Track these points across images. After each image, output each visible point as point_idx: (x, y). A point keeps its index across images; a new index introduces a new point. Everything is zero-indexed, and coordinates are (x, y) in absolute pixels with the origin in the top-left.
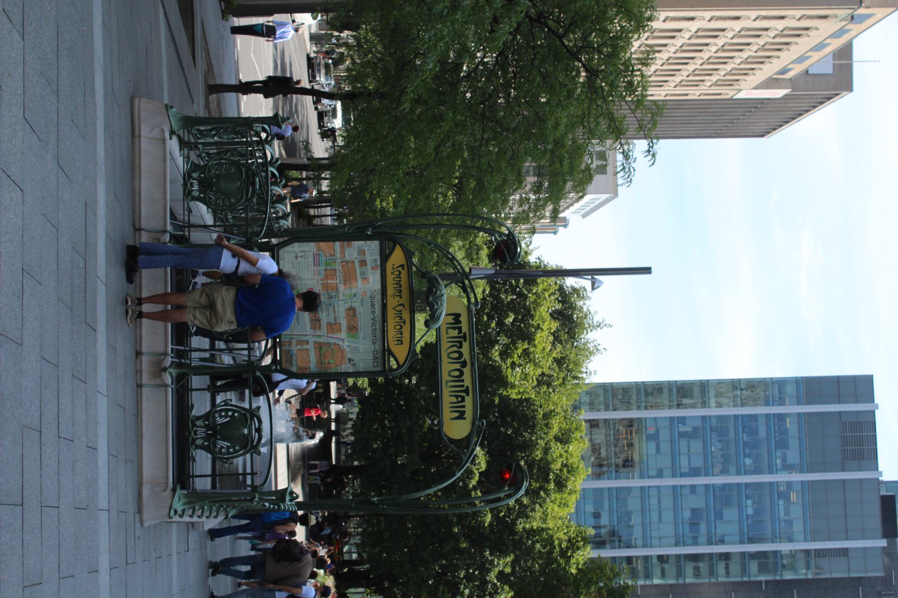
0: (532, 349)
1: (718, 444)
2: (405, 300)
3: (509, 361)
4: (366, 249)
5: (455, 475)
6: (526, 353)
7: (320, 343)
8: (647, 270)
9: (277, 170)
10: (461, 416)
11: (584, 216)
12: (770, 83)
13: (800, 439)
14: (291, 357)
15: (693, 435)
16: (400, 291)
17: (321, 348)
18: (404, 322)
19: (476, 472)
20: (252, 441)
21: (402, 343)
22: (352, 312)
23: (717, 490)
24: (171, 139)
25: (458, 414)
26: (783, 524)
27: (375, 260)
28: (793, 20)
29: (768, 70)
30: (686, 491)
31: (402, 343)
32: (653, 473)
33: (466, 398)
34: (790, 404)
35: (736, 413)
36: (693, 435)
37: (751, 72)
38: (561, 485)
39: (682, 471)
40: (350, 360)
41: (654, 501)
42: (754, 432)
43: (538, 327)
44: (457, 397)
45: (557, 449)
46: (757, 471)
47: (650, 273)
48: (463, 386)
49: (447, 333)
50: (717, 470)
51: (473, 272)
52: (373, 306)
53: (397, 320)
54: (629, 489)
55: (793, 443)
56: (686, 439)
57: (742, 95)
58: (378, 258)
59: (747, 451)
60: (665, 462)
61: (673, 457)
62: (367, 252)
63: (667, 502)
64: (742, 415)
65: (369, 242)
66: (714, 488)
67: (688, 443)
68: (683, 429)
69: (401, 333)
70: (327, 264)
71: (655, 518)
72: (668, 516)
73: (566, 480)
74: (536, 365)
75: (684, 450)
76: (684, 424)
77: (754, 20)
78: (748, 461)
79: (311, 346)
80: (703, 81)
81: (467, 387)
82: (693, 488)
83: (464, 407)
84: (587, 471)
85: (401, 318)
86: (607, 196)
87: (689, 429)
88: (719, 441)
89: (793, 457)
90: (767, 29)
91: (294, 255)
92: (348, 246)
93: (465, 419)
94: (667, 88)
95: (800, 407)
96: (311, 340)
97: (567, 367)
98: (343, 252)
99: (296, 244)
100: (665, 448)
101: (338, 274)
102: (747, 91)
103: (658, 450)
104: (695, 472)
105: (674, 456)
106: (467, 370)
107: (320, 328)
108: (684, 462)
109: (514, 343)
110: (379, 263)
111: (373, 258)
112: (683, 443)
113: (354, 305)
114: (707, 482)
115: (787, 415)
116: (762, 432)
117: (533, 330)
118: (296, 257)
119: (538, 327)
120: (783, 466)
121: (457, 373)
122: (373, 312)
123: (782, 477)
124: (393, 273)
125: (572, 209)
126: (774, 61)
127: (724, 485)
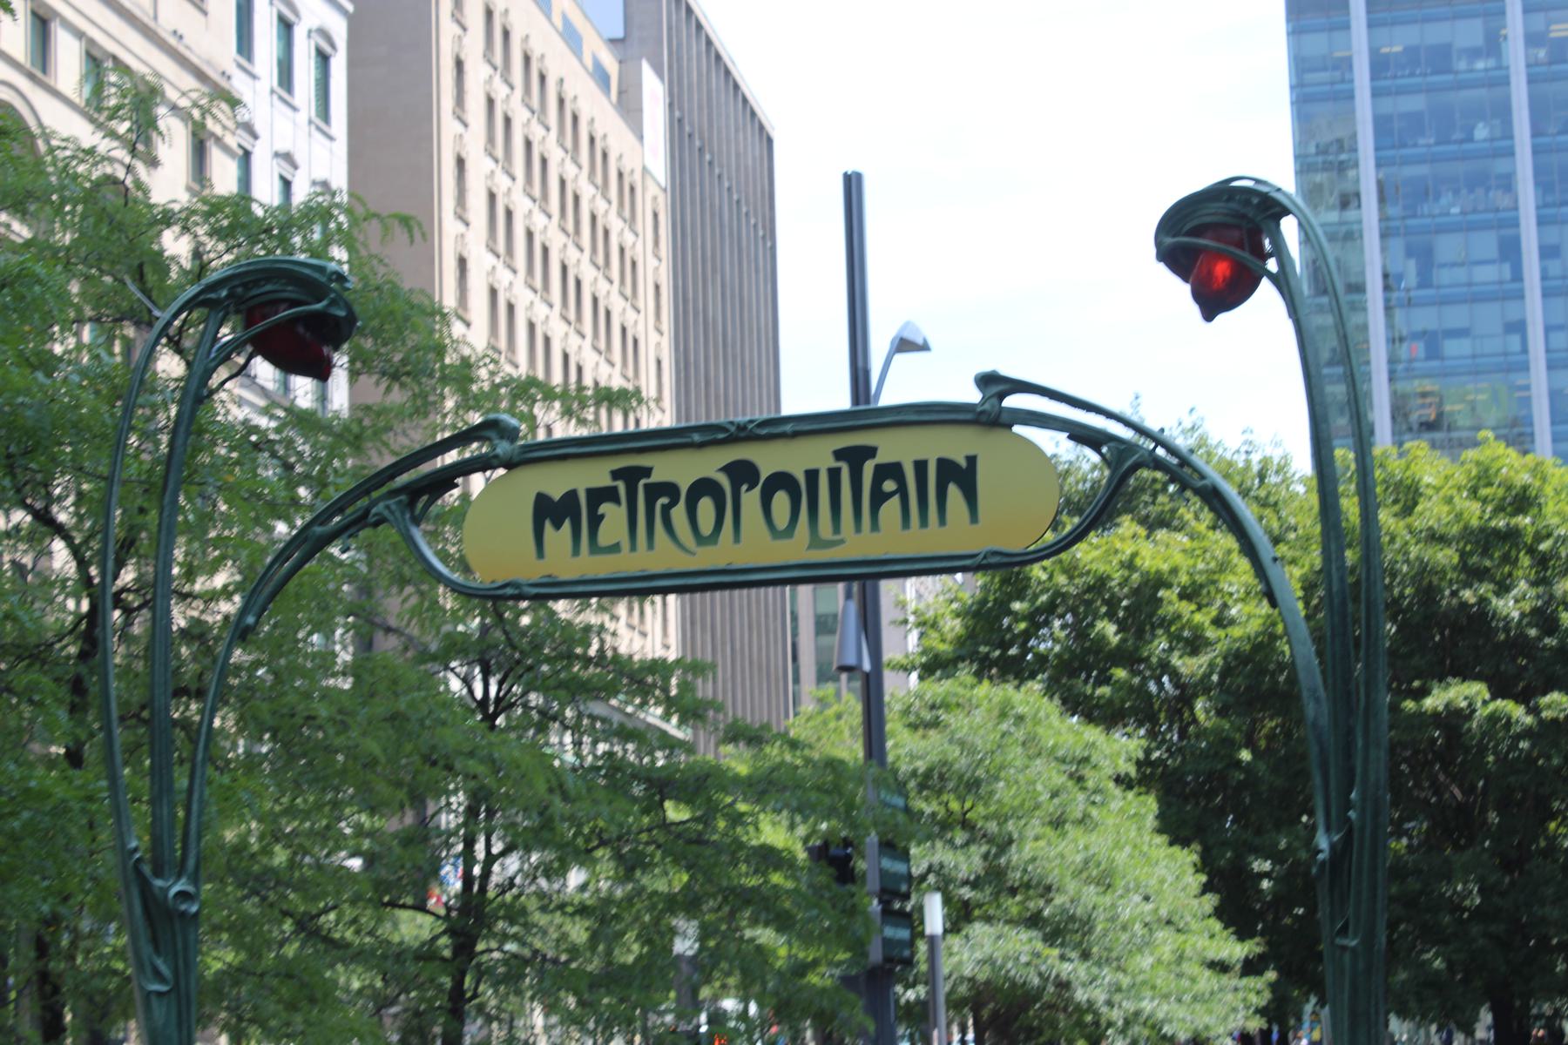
0: (1184, 579)
1: (1444, 201)
3: (1211, 633)
6: (1190, 594)
8: (852, 186)
12: (629, 106)
13: (1427, 20)
15: (1425, 258)
19: (1491, 707)
23: (1549, 199)
25: (953, 491)
28: (466, 40)
29: (596, 109)
30: (1555, 267)
32: (1514, 342)
33: (881, 458)
34: (1349, 47)
35: (1371, 163)
36: (1425, 258)
37: (599, 145)
38: (1522, 501)
39: (1507, 274)
42: (1415, 122)
43: (1130, 565)
44: (879, 498)
45: (1431, 512)
46: (1503, 112)
47: (859, 176)
48: (834, 474)
49: (615, 548)
50: (1504, 201)
51: (851, 660)
55: (1436, 34)
56: (1435, 271)
57: (658, 164)
59: (1457, 135)
60: (1489, 317)
64: (1377, 149)
66: (1546, 206)
67: (1444, 265)
68: (1411, 279)
73: (1509, 488)
74: (1224, 567)
75: (1460, 274)
76: (1400, 277)
77: (466, 125)
78: (1481, 132)
80: (622, 250)
81: (839, 454)
83: (921, 466)
84: (1486, 440)
87: (1411, 268)
88: (1437, 198)
89: (1469, 33)
90: (491, 102)
93: (972, 460)
94: (641, 327)
95: (1354, 24)
100: (1456, 317)
102: (648, 154)
104: (1510, 250)
105: (1476, 297)
108: (1487, 274)
109: (1165, 623)
112: (1444, 276)
114: (1533, 221)
115: (1374, 53)
116: (1415, 103)
117: (1135, 576)
119: (1130, 565)
120: (1488, 55)
121: (781, 500)
123: (1516, 55)
127: (1537, 184)
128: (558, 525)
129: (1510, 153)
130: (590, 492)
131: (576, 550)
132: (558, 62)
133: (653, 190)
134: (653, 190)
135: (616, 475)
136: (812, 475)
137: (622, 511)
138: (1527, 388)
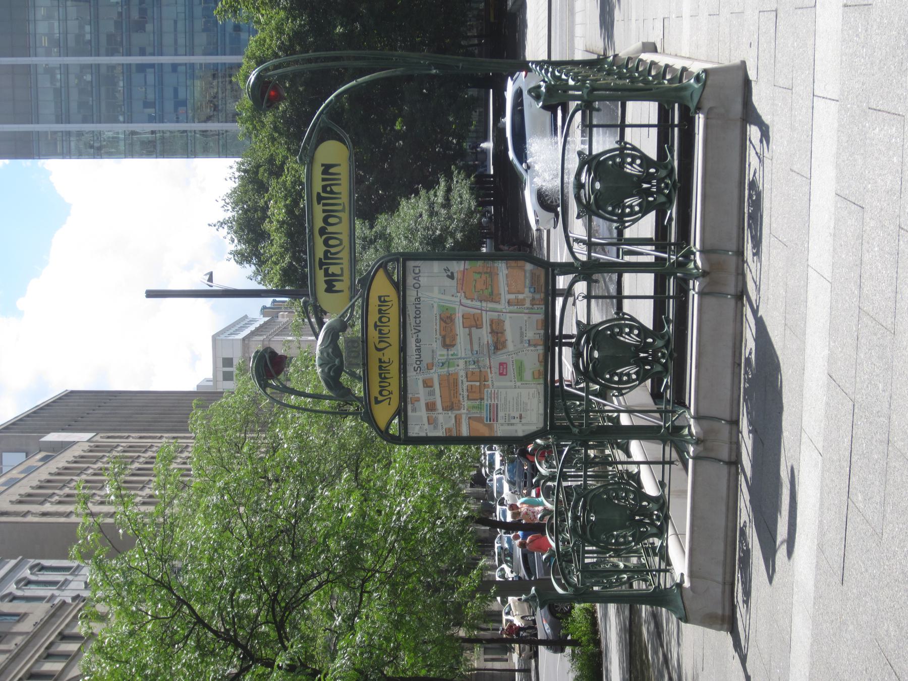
2: (374, 356)
4: (426, 426)
5: (336, 96)
7: (492, 301)
8: (151, 294)
9: (538, 470)
10: (327, 168)
11: (246, 317)
14: (532, 284)
16: (380, 368)
17: (492, 294)
18: (376, 326)
20: (589, 171)
21: (380, 297)
22: (448, 342)
24: (682, 575)
25: (331, 171)
26: (56, 14)
27: (414, 410)
29: (61, 461)
30: (149, 49)
31: (380, 297)
32: (180, 69)
33: (320, 191)
37: (78, 459)
39: (152, 70)
40: (451, 277)
41: (181, 41)
44: (332, 192)
48: (324, 205)
49: (342, 269)
52: (419, 350)
53: (386, 330)
54: (205, 54)
57: (87, 436)
58: (410, 413)
61: (161, 83)
62: (425, 420)
63: (168, 39)
65: (423, 434)
69: (380, 311)
70: (480, 407)
71: (181, 26)
72: (168, 25)
76: (150, 115)
79: (505, 296)
81: (319, 203)
82: (143, 52)
83: (323, 180)
85: (380, 331)
86: (13, 562)
89: (44, 82)
91: (523, 421)
92: (450, 430)
93: (323, 165)
96: (502, 306)
97: (254, 183)
98: (458, 419)
99: (520, 434)
100: (169, 93)
101: (465, 394)
103: (176, 91)
104: (142, 68)
106: (319, 223)
107: (492, 321)
108: (151, 78)
110: (409, 407)
111: (418, 414)
113: (445, 352)
118: (521, 418)
121: (331, 220)
122: (418, 341)
123: (55, 61)
124: (391, 393)
125: (257, 325)
126: (54, 470)
127: (112, 55)
128: (334, 286)
129: (98, 66)
130: (325, 276)
131: (342, 281)
132: (43, 474)
133: (98, 438)
134: (98, 438)
135: (321, 268)
136: (324, 211)
137: (331, 267)
138: (201, 64)
